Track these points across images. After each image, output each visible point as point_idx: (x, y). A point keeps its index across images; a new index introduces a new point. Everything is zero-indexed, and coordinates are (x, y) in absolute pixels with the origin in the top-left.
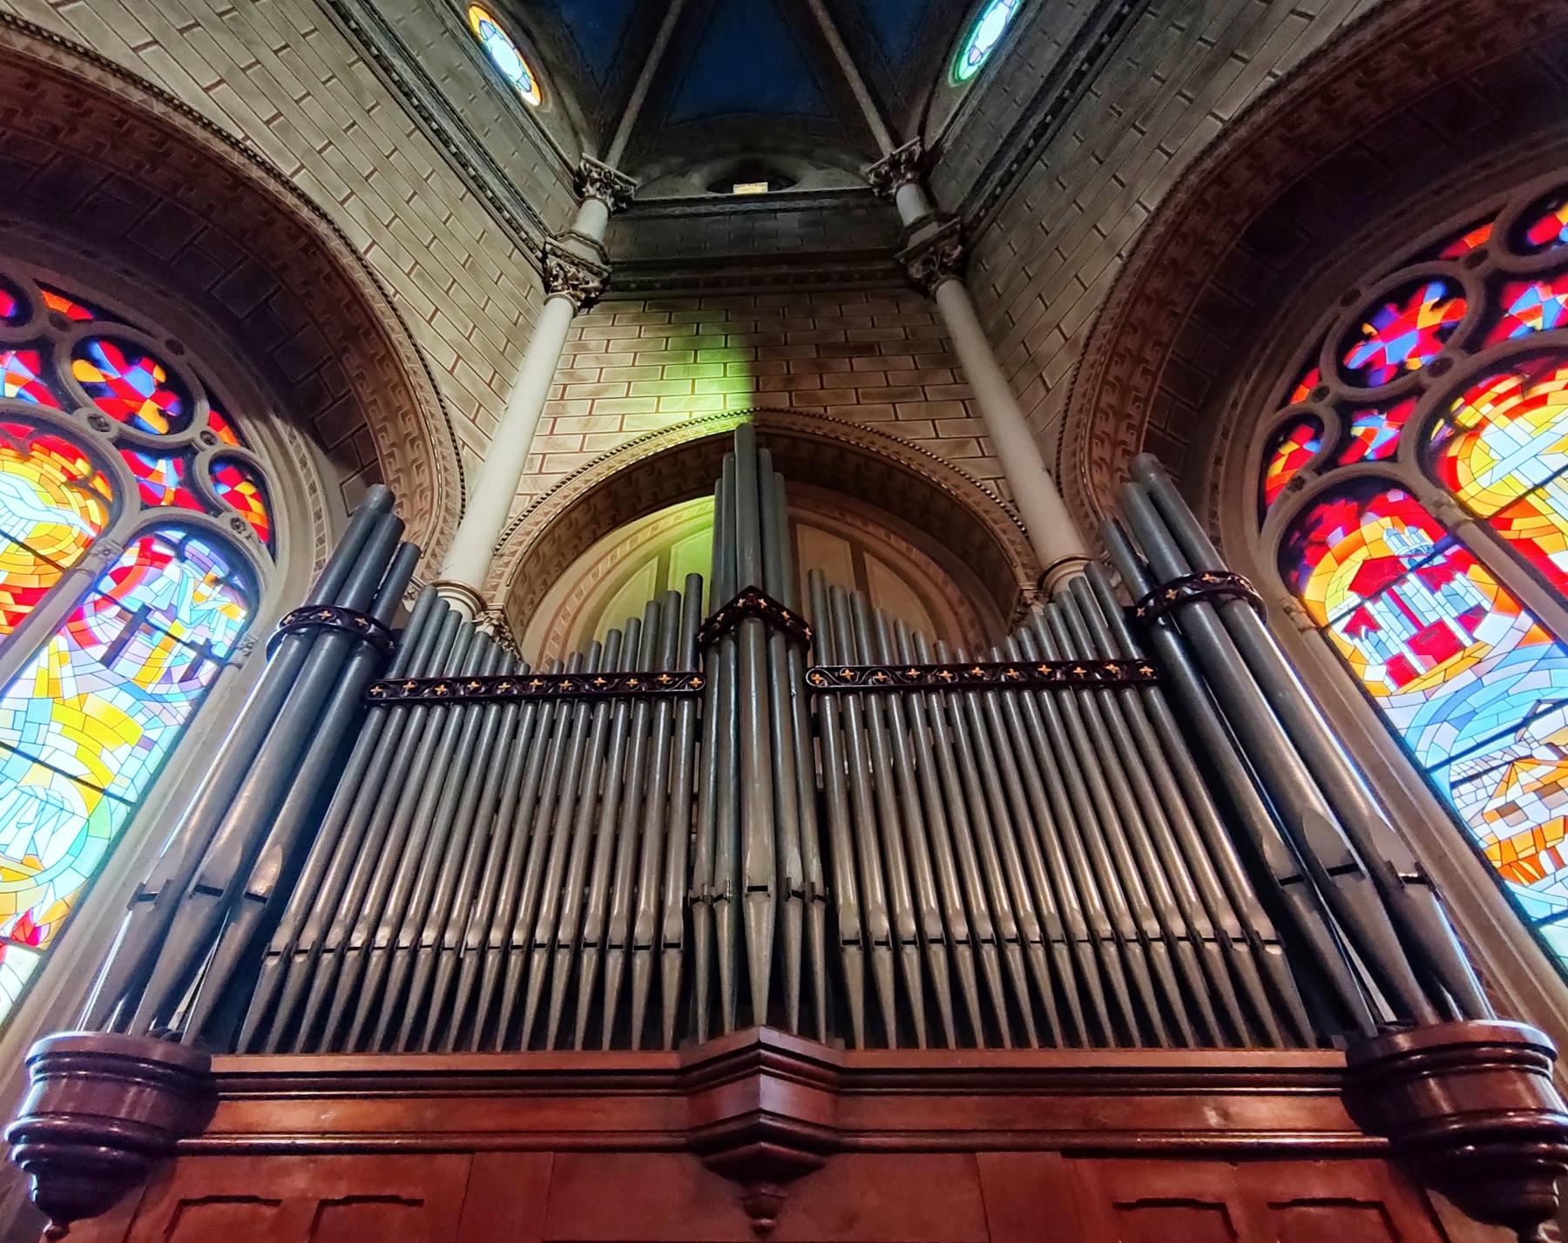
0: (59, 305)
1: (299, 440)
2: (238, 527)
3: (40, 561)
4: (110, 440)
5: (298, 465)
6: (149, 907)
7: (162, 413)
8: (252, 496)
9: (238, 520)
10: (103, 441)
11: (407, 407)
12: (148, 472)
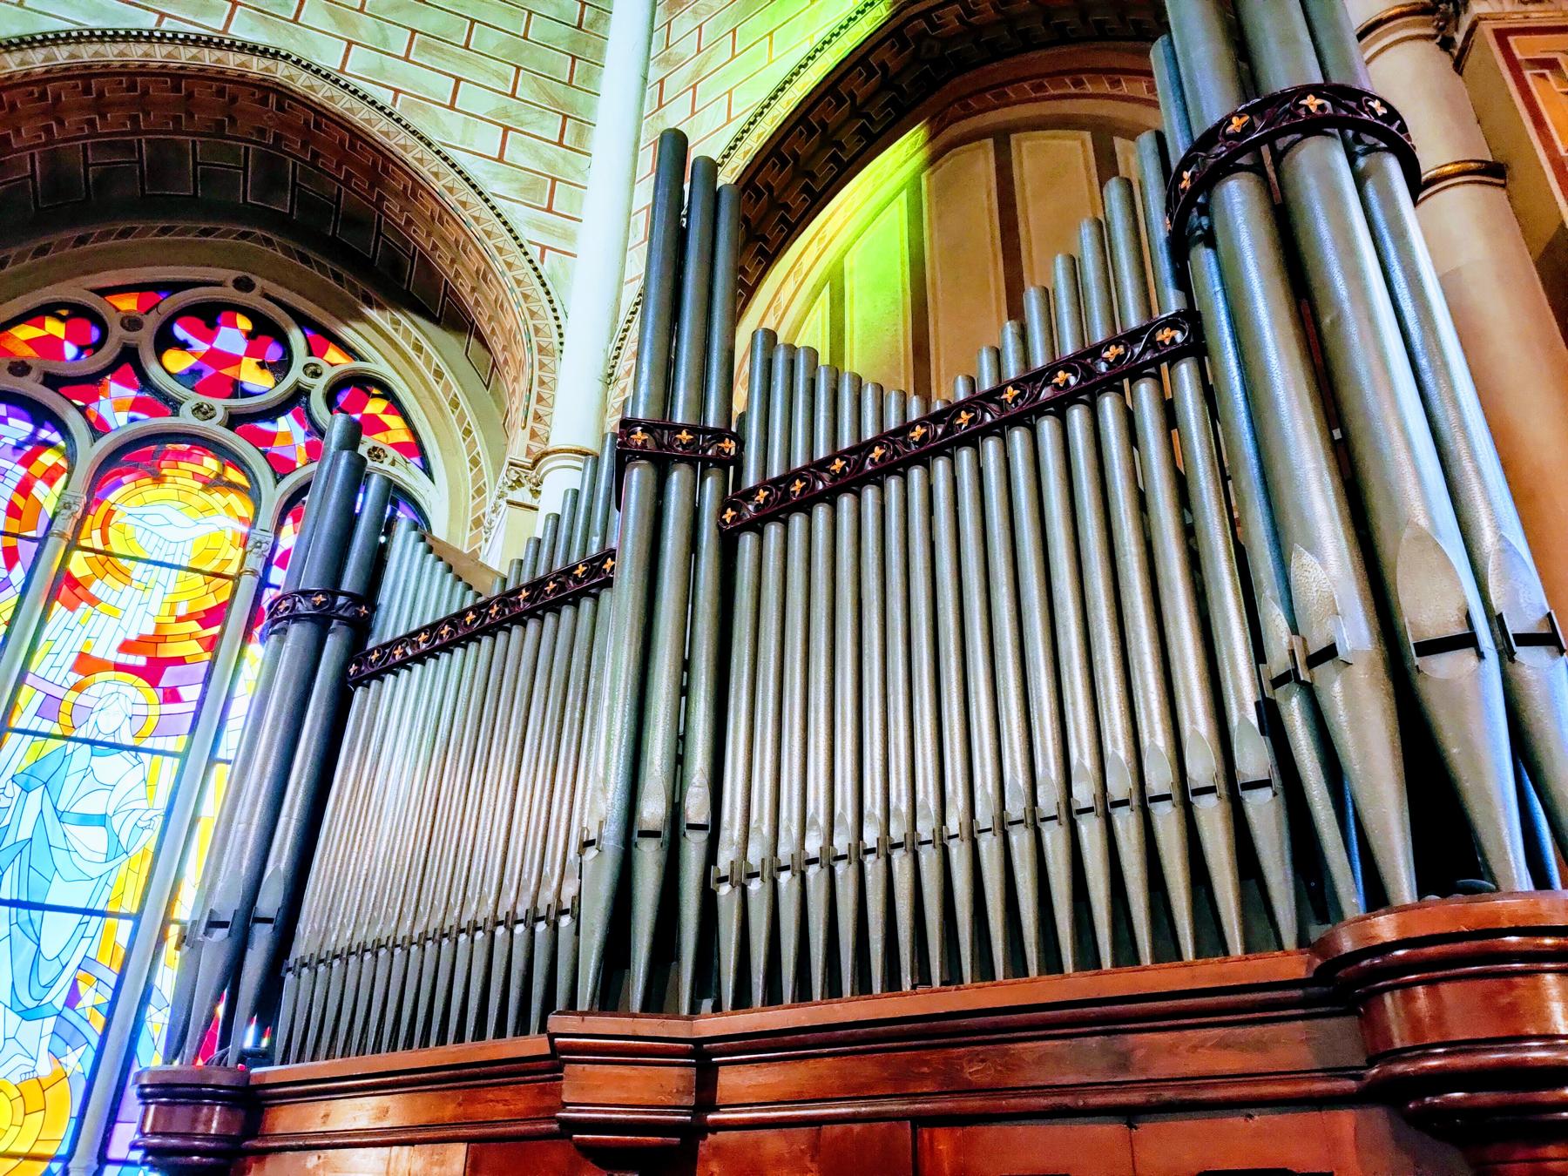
0: (128, 304)
1: (404, 321)
2: (378, 457)
3: (209, 578)
4: (220, 424)
5: (412, 353)
6: (221, 933)
7: (262, 365)
8: (386, 412)
9: (375, 449)
10: (215, 428)
11: (462, 238)
12: (270, 438)
